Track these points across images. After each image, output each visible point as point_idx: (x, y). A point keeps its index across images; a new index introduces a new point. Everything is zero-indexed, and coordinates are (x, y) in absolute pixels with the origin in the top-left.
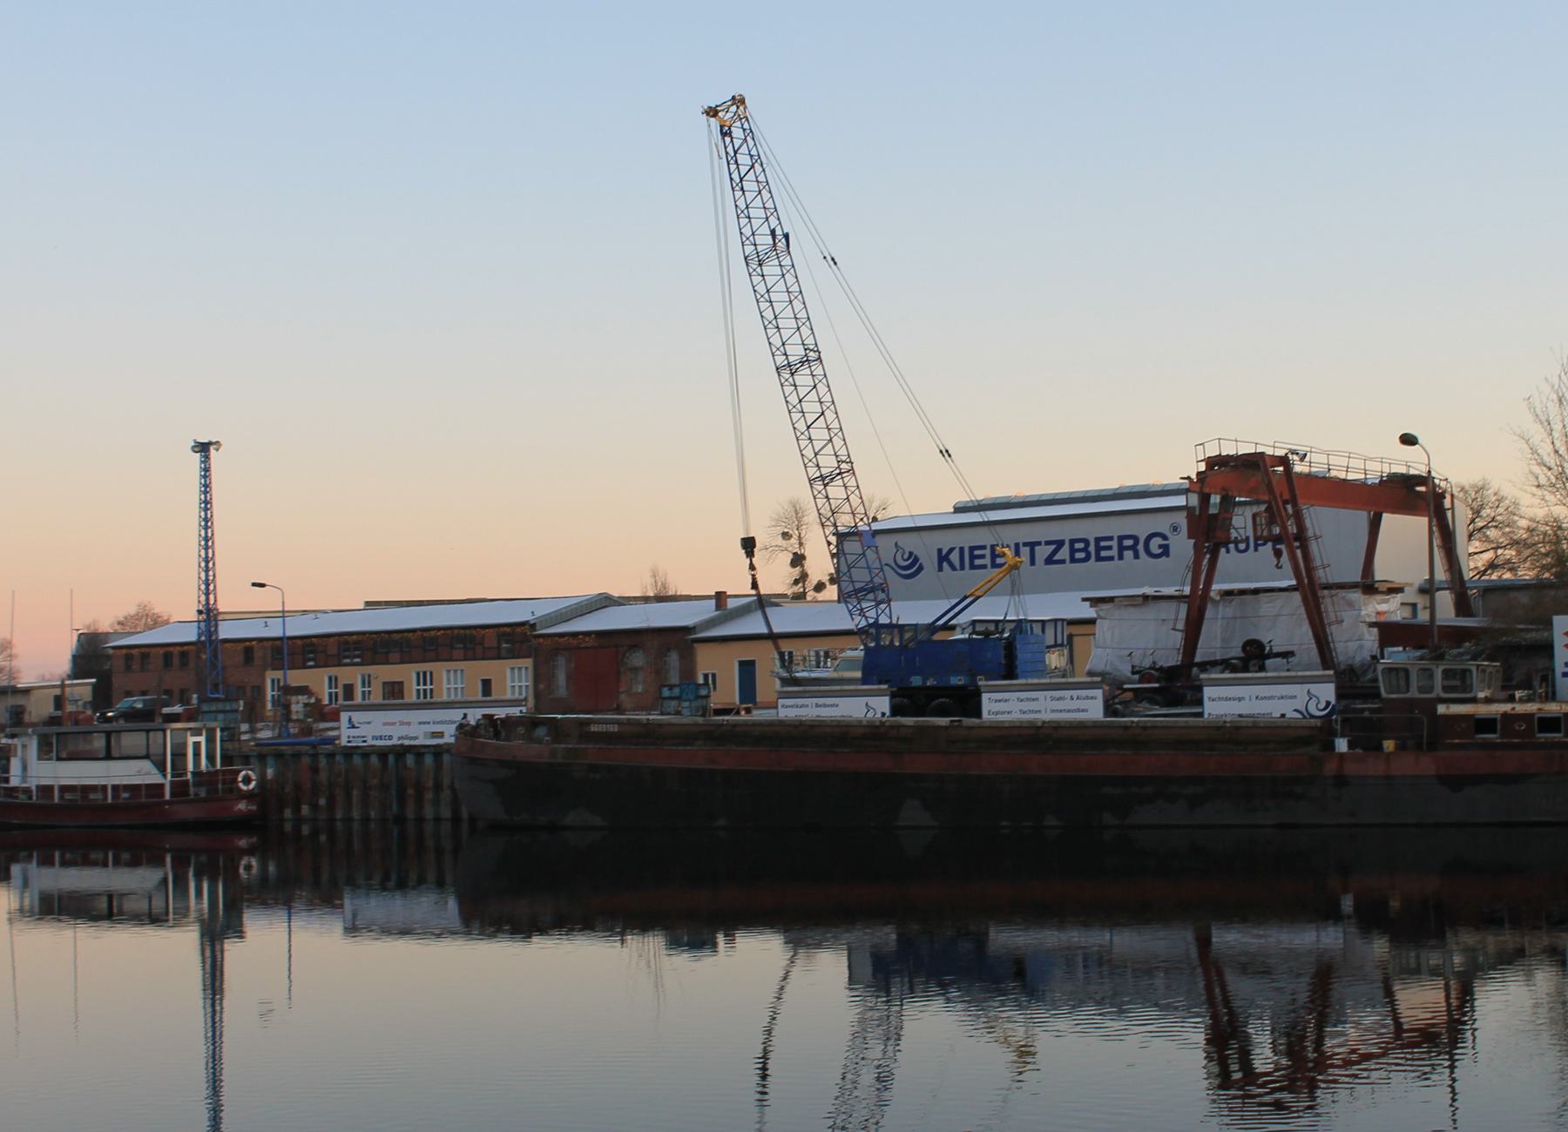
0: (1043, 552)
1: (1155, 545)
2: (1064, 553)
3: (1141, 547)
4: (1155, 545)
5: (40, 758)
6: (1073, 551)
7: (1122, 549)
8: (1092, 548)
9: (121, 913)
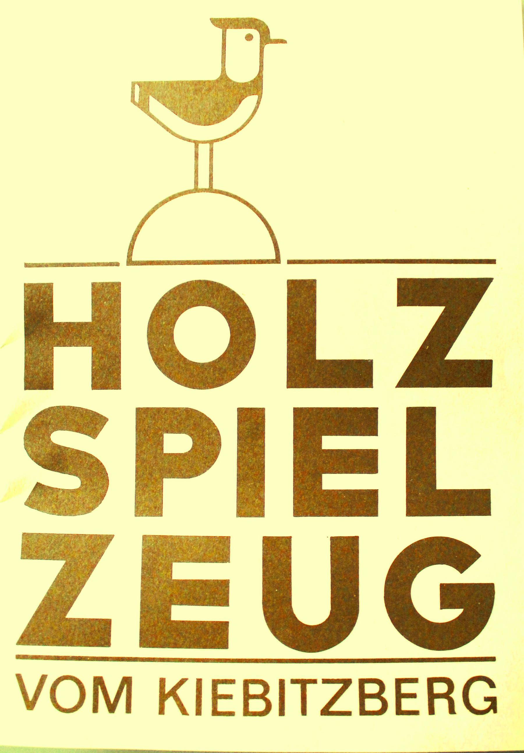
0: (319, 695)
1: (479, 694)
2: (350, 700)
3: (457, 695)
4: (479, 694)
5: (401, 282)
6: (363, 696)
7: (432, 696)
8: (390, 695)
9: (46, 378)
